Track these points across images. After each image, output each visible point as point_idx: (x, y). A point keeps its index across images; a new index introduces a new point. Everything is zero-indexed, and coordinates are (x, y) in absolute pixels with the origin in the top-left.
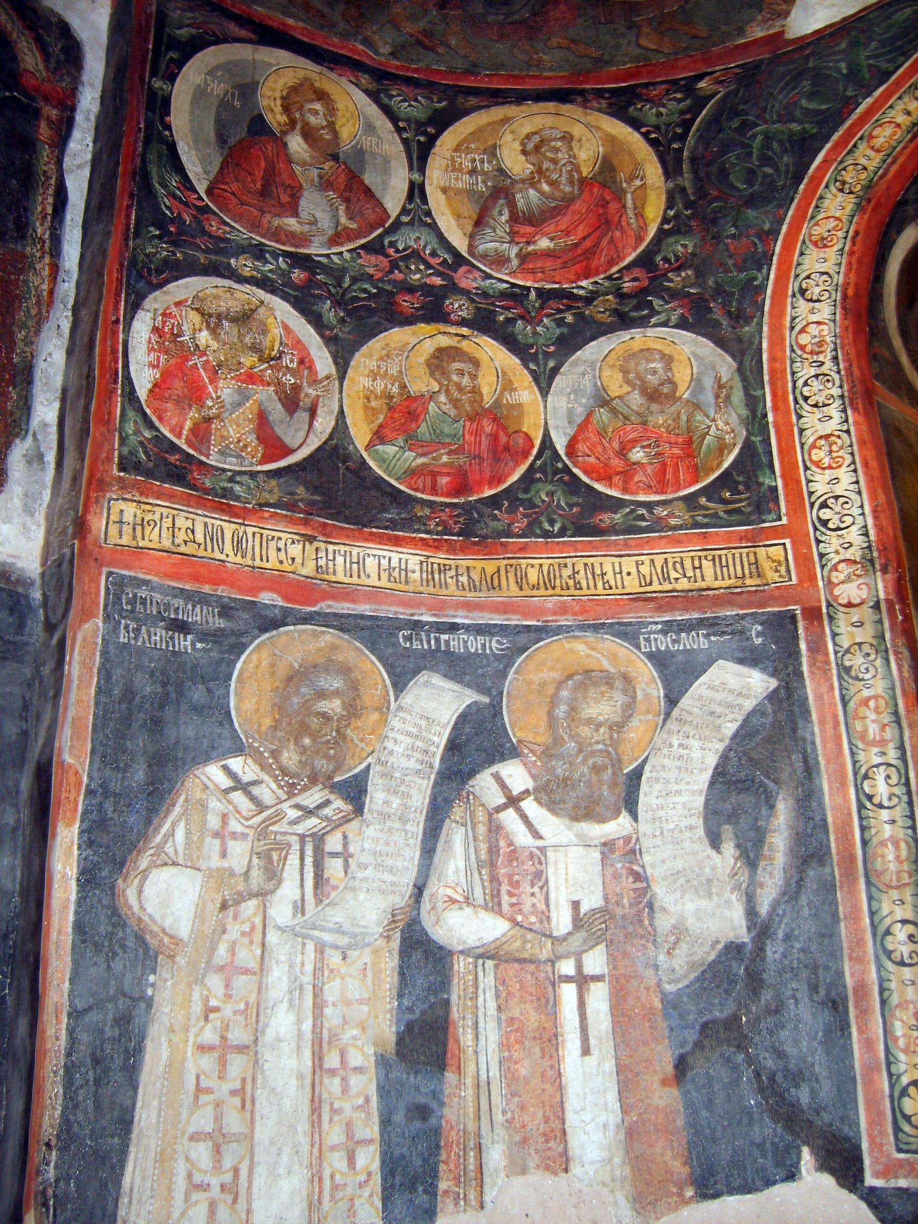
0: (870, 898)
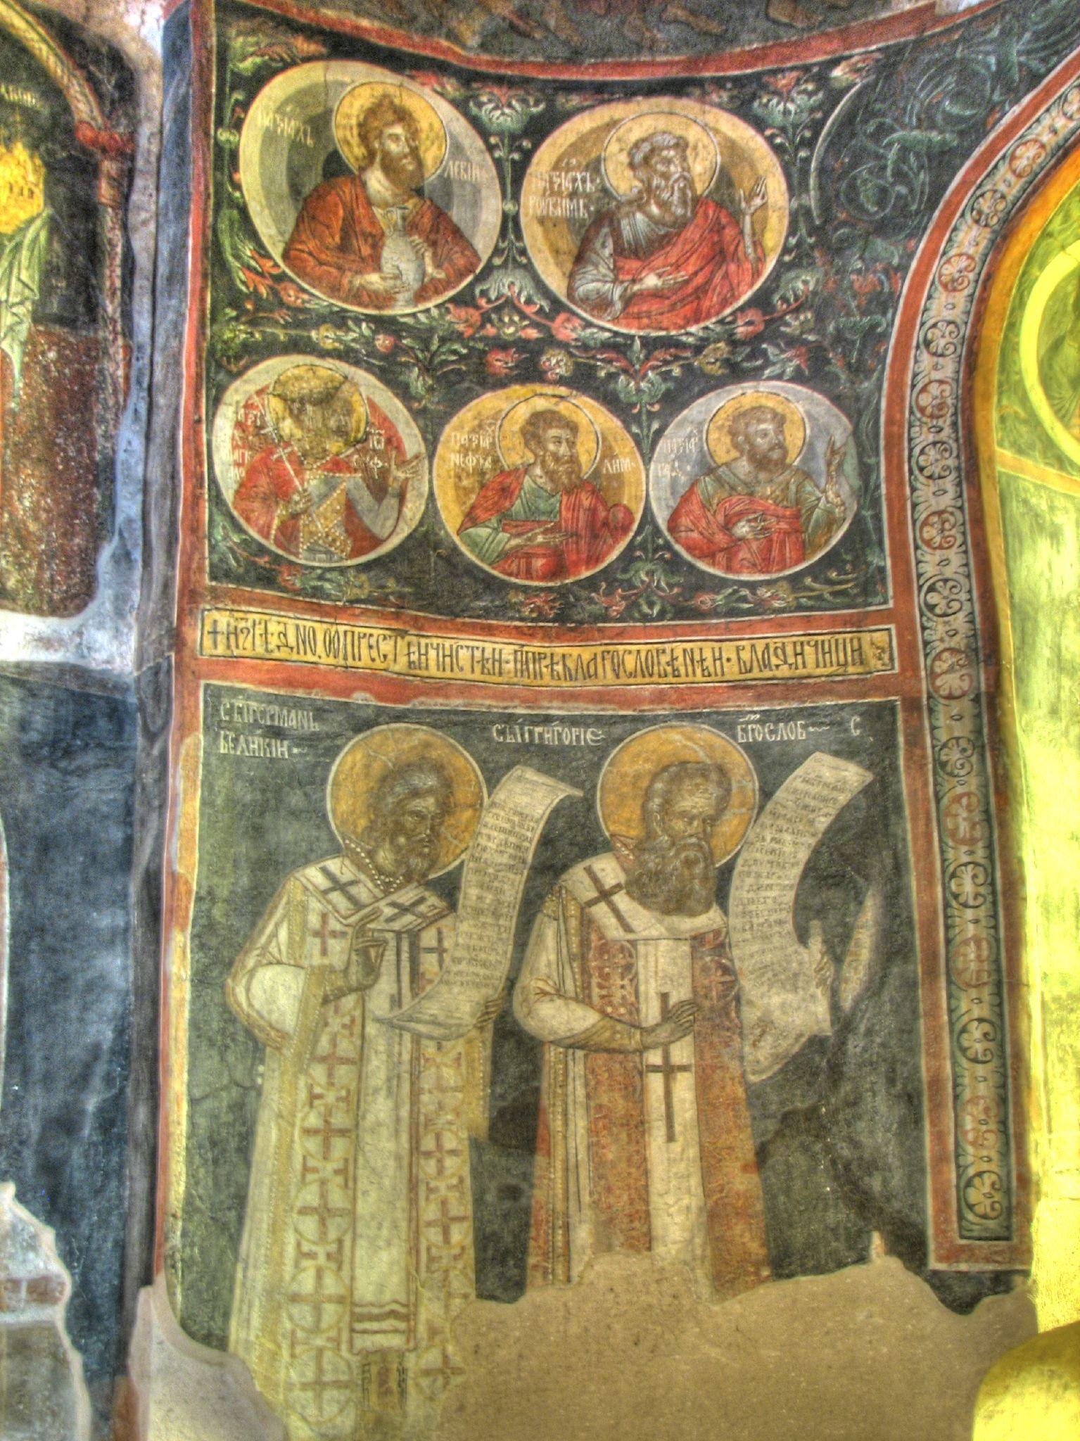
0: (950, 996)
